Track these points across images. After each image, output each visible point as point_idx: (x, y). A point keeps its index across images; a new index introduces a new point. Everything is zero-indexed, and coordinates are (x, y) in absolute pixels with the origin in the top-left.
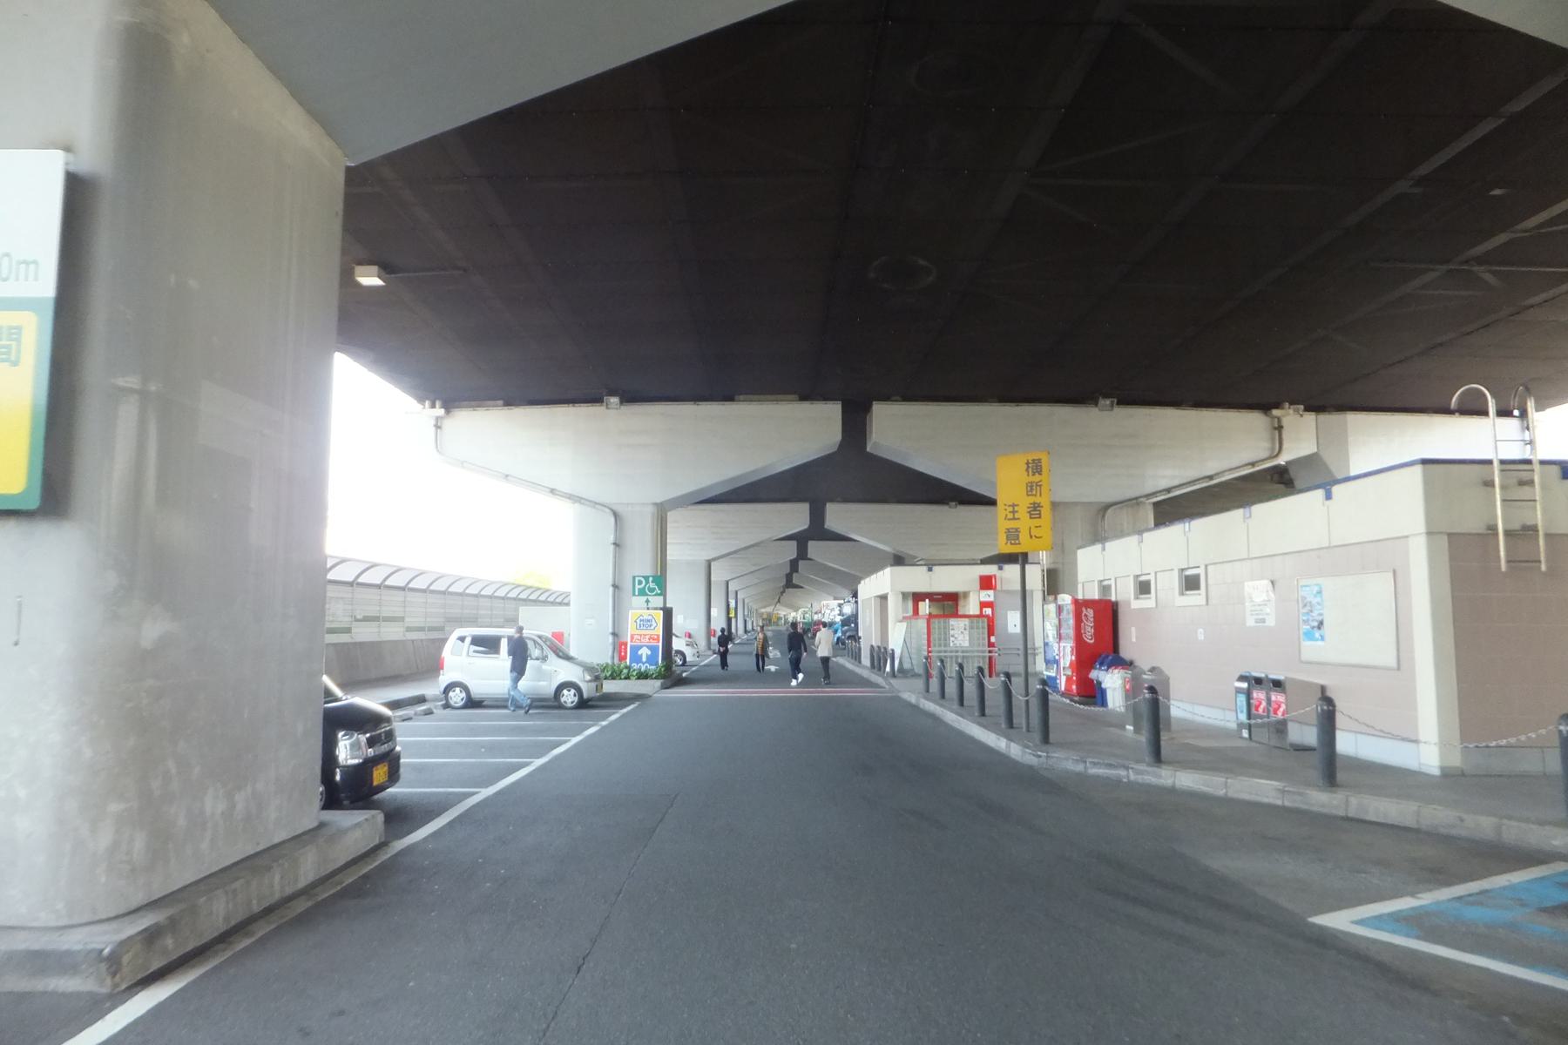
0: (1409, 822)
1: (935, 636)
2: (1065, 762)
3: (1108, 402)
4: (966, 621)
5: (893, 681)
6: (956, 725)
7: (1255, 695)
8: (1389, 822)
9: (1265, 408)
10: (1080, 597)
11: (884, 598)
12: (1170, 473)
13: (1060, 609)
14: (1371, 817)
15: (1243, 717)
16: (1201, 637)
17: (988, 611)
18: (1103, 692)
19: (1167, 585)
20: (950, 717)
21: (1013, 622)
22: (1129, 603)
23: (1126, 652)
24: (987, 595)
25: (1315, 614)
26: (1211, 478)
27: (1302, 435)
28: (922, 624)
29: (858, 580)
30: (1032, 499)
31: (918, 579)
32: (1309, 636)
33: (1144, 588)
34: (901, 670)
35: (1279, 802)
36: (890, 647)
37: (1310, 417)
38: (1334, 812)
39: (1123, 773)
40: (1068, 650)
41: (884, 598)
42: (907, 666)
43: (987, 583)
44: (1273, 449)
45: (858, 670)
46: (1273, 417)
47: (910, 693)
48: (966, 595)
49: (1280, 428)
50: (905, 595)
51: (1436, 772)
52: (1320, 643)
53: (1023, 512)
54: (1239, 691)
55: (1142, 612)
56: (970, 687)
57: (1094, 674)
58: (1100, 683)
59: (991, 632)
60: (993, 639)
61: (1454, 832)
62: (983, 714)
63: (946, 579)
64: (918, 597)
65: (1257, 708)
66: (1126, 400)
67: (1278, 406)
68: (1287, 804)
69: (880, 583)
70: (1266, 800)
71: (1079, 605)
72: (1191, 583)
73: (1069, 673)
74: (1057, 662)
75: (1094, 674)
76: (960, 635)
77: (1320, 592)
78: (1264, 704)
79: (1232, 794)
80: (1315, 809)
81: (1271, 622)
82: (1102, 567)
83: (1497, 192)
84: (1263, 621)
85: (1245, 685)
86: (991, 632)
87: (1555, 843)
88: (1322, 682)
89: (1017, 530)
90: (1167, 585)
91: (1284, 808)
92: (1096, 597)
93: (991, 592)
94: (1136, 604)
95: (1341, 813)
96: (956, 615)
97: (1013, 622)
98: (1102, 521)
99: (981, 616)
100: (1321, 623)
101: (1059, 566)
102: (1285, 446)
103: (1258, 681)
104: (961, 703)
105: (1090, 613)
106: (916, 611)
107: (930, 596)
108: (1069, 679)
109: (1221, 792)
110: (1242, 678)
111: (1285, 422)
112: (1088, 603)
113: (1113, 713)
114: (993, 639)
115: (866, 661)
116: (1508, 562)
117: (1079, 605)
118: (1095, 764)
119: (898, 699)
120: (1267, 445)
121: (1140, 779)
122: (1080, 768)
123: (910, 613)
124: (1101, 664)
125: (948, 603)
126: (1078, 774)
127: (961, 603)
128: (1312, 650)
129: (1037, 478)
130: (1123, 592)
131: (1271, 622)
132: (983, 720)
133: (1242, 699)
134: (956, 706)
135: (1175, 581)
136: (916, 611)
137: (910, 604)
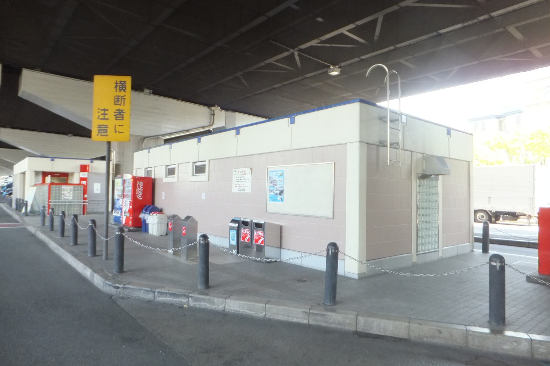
0: (402, 334)
1: (53, 194)
2: (138, 291)
3: (148, 91)
4: (72, 187)
5: (26, 219)
6: (56, 251)
7: (243, 231)
8: (388, 334)
9: (209, 105)
10: (135, 175)
11: (24, 173)
12: (170, 127)
13: (124, 182)
14: (375, 331)
15: (234, 243)
16: (203, 197)
17: (84, 182)
18: (146, 226)
19: (185, 172)
20: (53, 245)
21: (97, 188)
22: (162, 179)
23: (158, 204)
24: (84, 175)
25: (278, 187)
26: (187, 131)
27: (221, 117)
28: (46, 188)
29: (13, 164)
30: (118, 107)
31: (46, 165)
32: (273, 199)
33: (171, 172)
34: (31, 212)
35: (305, 322)
36: (26, 200)
37: (224, 112)
38: (347, 328)
39: (184, 300)
40: (128, 203)
41: (24, 173)
42: (36, 209)
43: (84, 168)
44: (210, 123)
45: (8, 211)
46: (212, 110)
47: (33, 226)
48: (72, 174)
49: (214, 114)
50: (37, 173)
51: (356, 277)
52: (281, 203)
53: (111, 115)
54: (231, 228)
55: (169, 184)
56: (68, 223)
57: (142, 216)
58: (145, 221)
59: (85, 192)
60: (86, 196)
61: (435, 341)
62: (76, 243)
63: (60, 166)
64: (45, 174)
65: (244, 238)
66: (155, 93)
67: (213, 106)
68: (311, 322)
69: (24, 166)
70: (295, 320)
71: (136, 180)
72: (199, 169)
73: (128, 215)
74: (121, 209)
75: (142, 216)
76: (67, 193)
77: (282, 175)
78: (249, 236)
79: (269, 315)
80: (333, 326)
81: (248, 190)
82: (144, 162)
83: (320, 19)
84: (244, 190)
85: (236, 225)
86: (85, 192)
87: (506, 347)
88: (281, 224)
89: (106, 126)
90: (185, 172)
91: (309, 326)
92: (143, 176)
93: (86, 173)
94: (165, 180)
95: (353, 329)
96: (66, 184)
97: (97, 188)
98: (142, 142)
99: (80, 184)
100: (281, 192)
101: (121, 163)
102: (215, 122)
103: (245, 223)
104: (63, 234)
105: (141, 184)
106: (44, 181)
107: (53, 174)
108: (127, 218)
109: (262, 315)
110: (233, 221)
111: (216, 112)
112: (141, 179)
113: (152, 236)
114: (86, 196)
115: (14, 206)
116: (390, 160)
117: (136, 180)
118: (161, 293)
119: (25, 230)
120: (208, 120)
121: (198, 304)
122: (150, 296)
123: (41, 182)
124: (146, 210)
125: (63, 177)
126: (149, 302)
127: (70, 178)
128: (273, 206)
129: (122, 93)
130: (159, 174)
131: (248, 190)
132: (76, 249)
133: (234, 233)
134: (58, 237)
135: (190, 168)
136: (44, 181)
137: (40, 178)
